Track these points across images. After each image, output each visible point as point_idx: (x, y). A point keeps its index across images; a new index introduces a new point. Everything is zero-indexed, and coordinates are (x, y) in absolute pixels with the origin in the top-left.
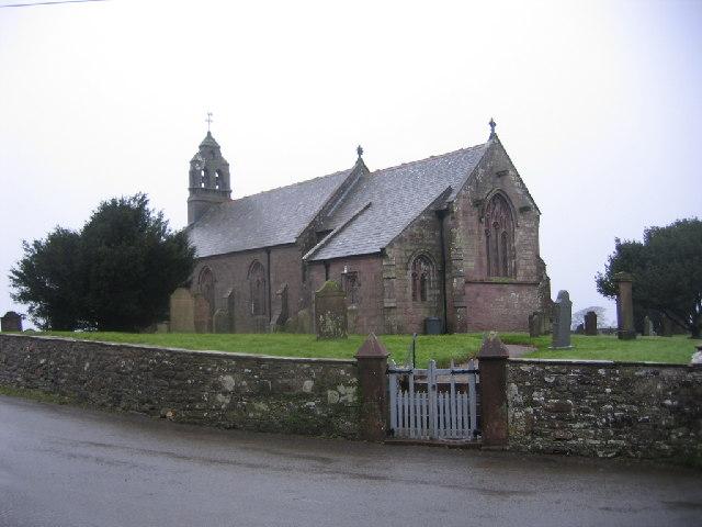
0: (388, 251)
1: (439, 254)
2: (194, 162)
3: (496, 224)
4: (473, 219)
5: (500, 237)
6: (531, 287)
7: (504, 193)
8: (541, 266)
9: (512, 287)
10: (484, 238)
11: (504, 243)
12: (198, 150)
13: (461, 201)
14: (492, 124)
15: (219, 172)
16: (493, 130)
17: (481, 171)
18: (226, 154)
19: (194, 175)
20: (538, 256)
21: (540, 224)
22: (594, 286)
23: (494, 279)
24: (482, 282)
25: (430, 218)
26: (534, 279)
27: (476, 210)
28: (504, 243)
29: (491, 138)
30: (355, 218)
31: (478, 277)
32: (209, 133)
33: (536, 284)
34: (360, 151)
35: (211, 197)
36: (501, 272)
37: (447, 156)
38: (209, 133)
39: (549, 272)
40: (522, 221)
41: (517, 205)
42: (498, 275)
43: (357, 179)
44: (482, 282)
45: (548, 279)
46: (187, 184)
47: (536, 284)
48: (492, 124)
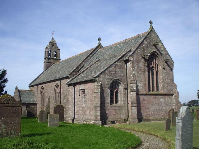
12: (48, 44)
29: (150, 28)
30: (93, 64)
34: (100, 40)
35: (52, 61)
45: (178, 92)
48: (151, 23)
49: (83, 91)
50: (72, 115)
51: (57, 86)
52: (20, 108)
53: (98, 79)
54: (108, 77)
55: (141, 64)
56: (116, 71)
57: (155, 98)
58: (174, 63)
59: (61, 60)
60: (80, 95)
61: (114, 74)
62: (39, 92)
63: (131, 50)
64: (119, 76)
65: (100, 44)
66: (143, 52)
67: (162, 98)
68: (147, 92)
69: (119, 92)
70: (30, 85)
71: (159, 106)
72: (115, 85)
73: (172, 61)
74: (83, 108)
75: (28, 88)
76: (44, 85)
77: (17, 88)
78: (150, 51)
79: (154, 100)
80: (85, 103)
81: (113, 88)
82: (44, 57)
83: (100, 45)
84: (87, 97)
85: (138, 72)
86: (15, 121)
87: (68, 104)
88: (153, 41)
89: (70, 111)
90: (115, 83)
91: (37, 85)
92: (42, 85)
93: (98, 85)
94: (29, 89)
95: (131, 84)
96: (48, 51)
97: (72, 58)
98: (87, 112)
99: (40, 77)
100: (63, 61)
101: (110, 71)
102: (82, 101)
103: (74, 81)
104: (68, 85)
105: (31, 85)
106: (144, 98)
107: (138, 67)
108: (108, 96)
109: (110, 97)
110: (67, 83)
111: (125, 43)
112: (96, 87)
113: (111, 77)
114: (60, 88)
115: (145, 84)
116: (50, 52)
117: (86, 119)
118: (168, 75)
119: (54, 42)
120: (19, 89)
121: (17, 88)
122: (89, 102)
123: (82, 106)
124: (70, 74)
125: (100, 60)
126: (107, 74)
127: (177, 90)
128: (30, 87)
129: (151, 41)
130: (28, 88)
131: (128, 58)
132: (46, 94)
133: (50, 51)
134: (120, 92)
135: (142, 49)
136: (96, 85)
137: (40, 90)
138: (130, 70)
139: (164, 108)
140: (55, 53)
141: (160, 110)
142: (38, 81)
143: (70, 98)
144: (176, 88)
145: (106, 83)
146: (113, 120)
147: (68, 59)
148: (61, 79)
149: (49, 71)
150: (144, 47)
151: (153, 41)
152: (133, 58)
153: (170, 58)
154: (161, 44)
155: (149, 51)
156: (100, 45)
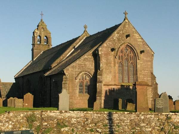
4: (111, 58)
55: (110, 57)
56: (85, 65)
61: (82, 67)
85: (107, 65)
101: (78, 65)
108: (77, 87)
118: (145, 67)
142: (26, 74)
150: (114, 40)
155: (121, 44)
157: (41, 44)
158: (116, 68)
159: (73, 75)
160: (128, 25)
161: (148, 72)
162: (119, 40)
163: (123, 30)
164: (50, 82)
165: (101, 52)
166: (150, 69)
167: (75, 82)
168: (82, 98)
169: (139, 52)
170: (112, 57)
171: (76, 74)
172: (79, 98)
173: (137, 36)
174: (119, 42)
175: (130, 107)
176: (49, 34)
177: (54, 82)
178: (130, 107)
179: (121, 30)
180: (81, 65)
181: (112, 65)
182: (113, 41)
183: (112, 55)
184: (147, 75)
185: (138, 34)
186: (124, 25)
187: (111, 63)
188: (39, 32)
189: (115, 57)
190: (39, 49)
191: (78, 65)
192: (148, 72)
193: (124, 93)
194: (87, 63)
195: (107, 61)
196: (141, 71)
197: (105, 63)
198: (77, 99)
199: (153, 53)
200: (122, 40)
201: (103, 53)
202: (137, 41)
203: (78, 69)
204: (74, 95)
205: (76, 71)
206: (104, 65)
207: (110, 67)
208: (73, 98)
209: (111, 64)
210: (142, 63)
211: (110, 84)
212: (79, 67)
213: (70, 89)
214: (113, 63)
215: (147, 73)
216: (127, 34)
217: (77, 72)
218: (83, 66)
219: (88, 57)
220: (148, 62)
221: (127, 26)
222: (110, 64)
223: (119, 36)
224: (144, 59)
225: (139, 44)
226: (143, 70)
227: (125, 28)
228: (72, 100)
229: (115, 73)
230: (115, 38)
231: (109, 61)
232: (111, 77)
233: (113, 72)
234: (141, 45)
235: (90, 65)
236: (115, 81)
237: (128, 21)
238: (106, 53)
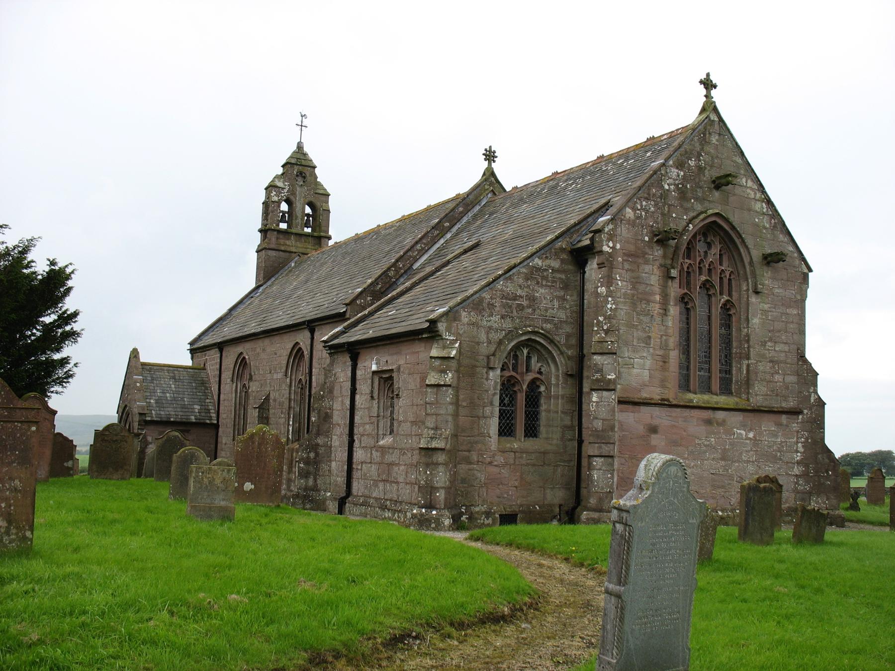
0: (441, 327)
1: (573, 341)
2: (270, 188)
3: (706, 286)
4: (652, 275)
5: (716, 311)
6: (784, 418)
7: (726, 220)
8: (809, 376)
9: (738, 417)
10: (674, 311)
11: (727, 324)
12: (280, 171)
13: (624, 231)
14: (708, 84)
15: (311, 205)
16: (707, 96)
17: (674, 172)
18: (323, 176)
19: (268, 207)
20: (802, 357)
21: (810, 292)
22: (81, 309)
23: (696, 398)
24: (664, 404)
25: (556, 264)
26: (791, 404)
27: (658, 252)
28: (727, 324)
29: (703, 110)
30: (448, 262)
31: (654, 393)
32: (300, 147)
33: (794, 412)
34: (490, 156)
35: (292, 244)
36: (715, 385)
37: (625, 154)
38: (300, 147)
39: (824, 390)
40: (767, 279)
41: (756, 248)
42: (708, 390)
43: (311, 161)
44: (664, 404)
45: (821, 404)
46: (257, 222)
47: (794, 412)
48: (708, 84)
49: (386, 379)
50: (341, 480)
51: (297, 354)
52: (34, 428)
53: (448, 329)
54: (495, 320)
55: (647, 268)
56: (532, 299)
57: (709, 422)
58: (810, 270)
59: (331, 243)
60: (376, 395)
61: (521, 308)
62: (227, 376)
63: (606, 206)
64: (547, 321)
65: (493, 174)
66: (663, 214)
67: (743, 426)
68: (672, 393)
69: (542, 389)
70: (191, 344)
71: (723, 458)
72: (529, 358)
73: (804, 260)
74: (383, 450)
75: (186, 360)
76: (244, 349)
77: (135, 354)
78: (694, 210)
79: (702, 429)
80: (392, 432)
81: (515, 368)
82: (260, 226)
83: (490, 176)
84: (402, 404)
85: (634, 305)
86: (11, 479)
87: (328, 434)
88: (712, 166)
89: (334, 464)
90: (525, 351)
91: (221, 346)
92: (239, 349)
93: (443, 354)
94: (189, 363)
95: (595, 357)
96: (276, 199)
97: (376, 233)
98: (399, 473)
99: (239, 310)
100: (338, 245)
101: (503, 297)
102: (381, 424)
103: (356, 335)
104: (331, 347)
105: (195, 346)
106: (656, 422)
107: (636, 282)
108: (491, 404)
109: (497, 410)
110: (324, 342)
111: (592, 173)
112: (437, 363)
113: (508, 325)
114: (308, 365)
115: (665, 361)
116: (284, 207)
117: (391, 500)
118: (778, 325)
119: (304, 163)
120: (143, 359)
121: (135, 354)
122: (406, 428)
123: (381, 443)
124: (347, 305)
125: (476, 246)
126: (491, 306)
127: (816, 392)
128: (193, 351)
129: (700, 169)
130: (186, 360)
131: (588, 242)
132: (254, 387)
133: (288, 201)
134: (548, 389)
135: (656, 205)
136: (435, 352)
137: (232, 366)
138: (597, 295)
139: (751, 468)
140: (308, 210)
141: (731, 477)
142: (228, 332)
143: (337, 406)
144: (815, 385)
145: (484, 349)
146: (509, 511)
147: (358, 239)
148: (311, 325)
149: (275, 287)
150: (665, 195)
151: (712, 166)
152: (653, 231)
153: (791, 249)
154: (750, 183)
155: (692, 214)
156: (490, 176)
157: (294, 230)
158: (670, 324)
159: (478, 343)
160: (720, 134)
161: (786, 348)
162: (683, 194)
163: (699, 155)
164: (349, 374)
165: (611, 244)
166: (795, 337)
167: (487, 379)
168: (512, 461)
169: (756, 254)
170: (657, 271)
171: (489, 342)
172: (500, 459)
173: (751, 188)
174: (682, 206)
175: (810, 528)
176: (323, 198)
177: (374, 373)
178: (810, 528)
179: (691, 150)
180: (515, 298)
181: (656, 308)
182: (661, 197)
183: (657, 263)
184: (786, 363)
185: (752, 180)
186: (705, 135)
187: (652, 298)
188: (287, 188)
189: (668, 272)
190: (283, 248)
191: (503, 297)
192: (786, 348)
193: (697, 441)
194: (542, 291)
195: (634, 288)
196: (764, 344)
197: (625, 294)
198: (490, 463)
199: (806, 271)
200: (696, 199)
201: (618, 246)
202: (749, 210)
203: (503, 317)
204: (476, 443)
205: (490, 328)
206: (621, 306)
207: (646, 319)
208: (475, 457)
209: (652, 305)
210: (766, 307)
211: (645, 395)
212: (504, 306)
213: (462, 411)
214: (658, 298)
215: (783, 355)
216: (715, 173)
217: (496, 330)
218: (525, 303)
219: (548, 262)
220: (790, 307)
221: (714, 139)
222: (648, 302)
223: (684, 176)
224: (777, 290)
225: (757, 225)
226: (771, 340)
227: (707, 148)
228: (468, 467)
229: (664, 347)
230: (666, 187)
231: (641, 288)
232: (648, 363)
233: (655, 341)
234: (765, 228)
235: (556, 303)
236: (663, 384)
237: (716, 119)
238: (632, 248)
